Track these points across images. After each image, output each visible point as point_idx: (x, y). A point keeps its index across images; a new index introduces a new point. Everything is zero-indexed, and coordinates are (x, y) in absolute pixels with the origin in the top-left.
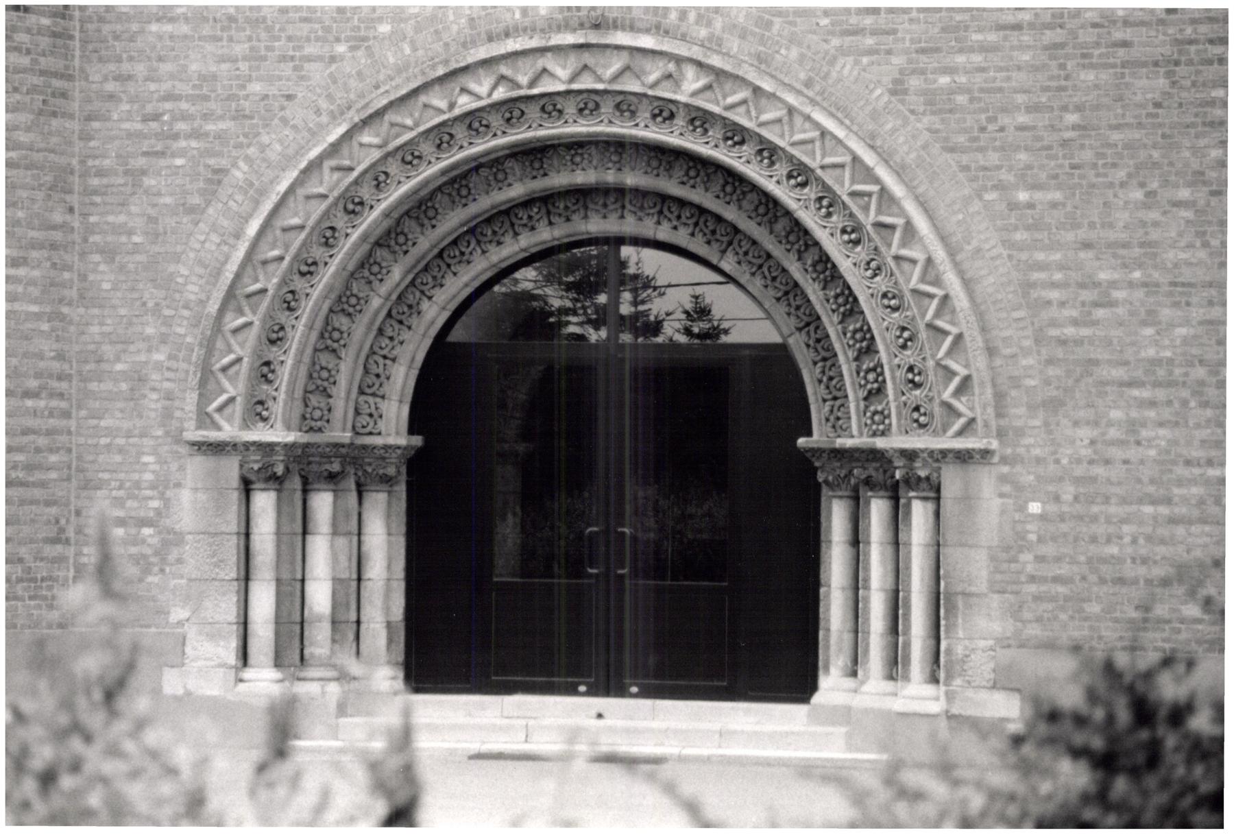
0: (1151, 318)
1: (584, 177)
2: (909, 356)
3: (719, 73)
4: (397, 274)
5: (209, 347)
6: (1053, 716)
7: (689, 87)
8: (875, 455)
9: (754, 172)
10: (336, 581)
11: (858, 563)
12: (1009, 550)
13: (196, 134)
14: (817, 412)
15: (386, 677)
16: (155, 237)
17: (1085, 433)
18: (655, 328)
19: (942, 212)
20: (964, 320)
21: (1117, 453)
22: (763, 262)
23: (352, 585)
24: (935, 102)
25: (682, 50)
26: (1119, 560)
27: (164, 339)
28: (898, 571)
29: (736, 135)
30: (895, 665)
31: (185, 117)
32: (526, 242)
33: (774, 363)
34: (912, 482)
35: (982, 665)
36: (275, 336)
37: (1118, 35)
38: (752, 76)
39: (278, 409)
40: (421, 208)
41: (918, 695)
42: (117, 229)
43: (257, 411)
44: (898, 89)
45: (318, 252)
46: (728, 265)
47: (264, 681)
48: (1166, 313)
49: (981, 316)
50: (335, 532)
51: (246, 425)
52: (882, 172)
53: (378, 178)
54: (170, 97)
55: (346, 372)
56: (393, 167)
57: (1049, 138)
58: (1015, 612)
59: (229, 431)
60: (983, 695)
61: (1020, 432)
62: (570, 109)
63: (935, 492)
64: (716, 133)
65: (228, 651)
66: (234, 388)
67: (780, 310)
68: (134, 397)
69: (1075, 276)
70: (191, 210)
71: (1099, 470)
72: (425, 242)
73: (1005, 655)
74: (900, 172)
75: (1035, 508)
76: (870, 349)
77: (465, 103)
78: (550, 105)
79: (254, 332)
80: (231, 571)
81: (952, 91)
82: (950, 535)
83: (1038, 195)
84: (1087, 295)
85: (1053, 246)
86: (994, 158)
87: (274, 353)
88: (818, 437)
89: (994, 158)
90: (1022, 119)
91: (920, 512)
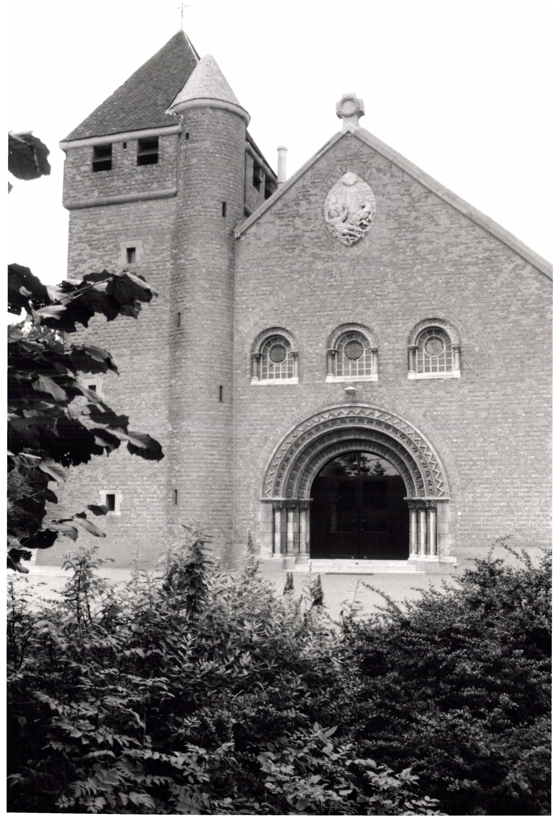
0: (486, 468)
1: (351, 437)
2: (429, 478)
3: (384, 412)
4: (307, 460)
5: (265, 479)
6: (471, 574)
7: (377, 415)
8: (421, 501)
9: (392, 435)
10: (294, 533)
11: (418, 527)
12: (453, 524)
13: (262, 429)
14: (408, 491)
15: (305, 557)
16: (252, 452)
17: (472, 495)
18: (368, 470)
19: (435, 444)
20: (441, 470)
21: (478, 500)
22: (395, 456)
23: (298, 533)
24: (434, 418)
25: (374, 407)
26: (480, 525)
27: (254, 477)
28: (427, 529)
29: (388, 427)
30: (427, 551)
31: (259, 425)
32: (337, 452)
33: (398, 478)
34: (430, 508)
35: (447, 551)
36: (280, 476)
37: (475, 403)
38: (391, 412)
39: (281, 492)
40: (312, 445)
41: (432, 558)
42: (244, 451)
43: (276, 493)
44: (425, 415)
45: (289, 456)
46: (386, 457)
47: (278, 556)
48: (489, 467)
49: (445, 468)
50: (294, 522)
51: (273, 496)
52: (422, 435)
53: (302, 438)
54: (256, 420)
55: (296, 484)
56: (306, 436)
57: (460, 426)
58: (455, 538)
59: (270, 497)
60: (447, 558)
61: (456, 495)
62: (348, 421)
63: (435, 510)
64: (383, 426)
65: (270, 549)
66: (271, 487)
67: (399, 468)
68: (248, 490)
69: (467, 458)
70: (260, 447)
71: (475, 504)
72: (313, 453)
73: (453, 549)
74: (426, 435)
75: (460, 514)
76: (420, 477)
77: (322, 420)
78: (343, 420)
79: (275, 476)
80: (270, 530)
81: (437, 416)
82: (439, 520)
83: (458, 440)
84: (470, 463)
85: (462, 451)
86: (447, 431)
87: (279, 480)
88: (408, 497)
89: (447, 431)
90: (454, 422)
91: (432, 515)
